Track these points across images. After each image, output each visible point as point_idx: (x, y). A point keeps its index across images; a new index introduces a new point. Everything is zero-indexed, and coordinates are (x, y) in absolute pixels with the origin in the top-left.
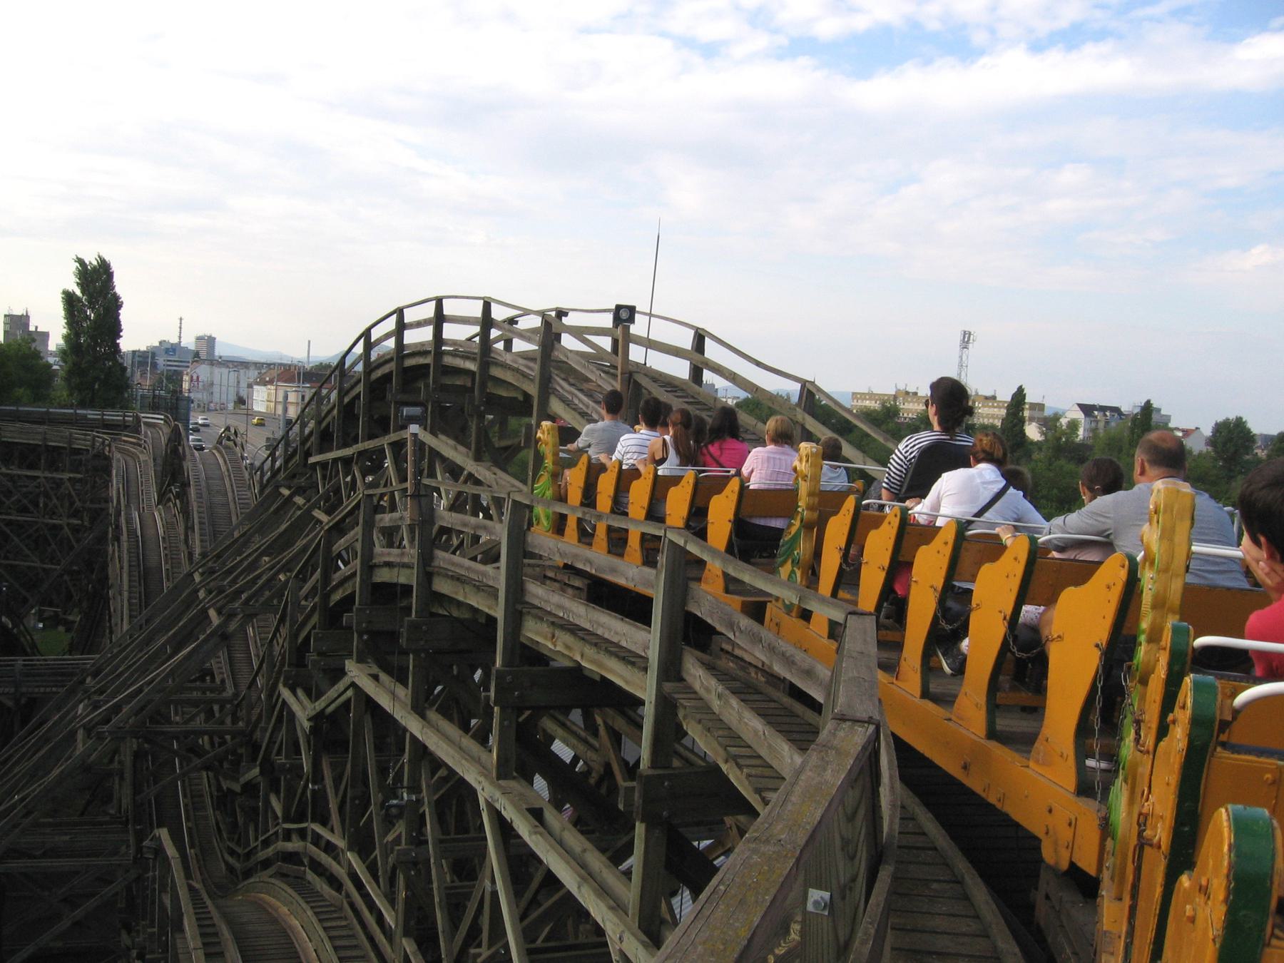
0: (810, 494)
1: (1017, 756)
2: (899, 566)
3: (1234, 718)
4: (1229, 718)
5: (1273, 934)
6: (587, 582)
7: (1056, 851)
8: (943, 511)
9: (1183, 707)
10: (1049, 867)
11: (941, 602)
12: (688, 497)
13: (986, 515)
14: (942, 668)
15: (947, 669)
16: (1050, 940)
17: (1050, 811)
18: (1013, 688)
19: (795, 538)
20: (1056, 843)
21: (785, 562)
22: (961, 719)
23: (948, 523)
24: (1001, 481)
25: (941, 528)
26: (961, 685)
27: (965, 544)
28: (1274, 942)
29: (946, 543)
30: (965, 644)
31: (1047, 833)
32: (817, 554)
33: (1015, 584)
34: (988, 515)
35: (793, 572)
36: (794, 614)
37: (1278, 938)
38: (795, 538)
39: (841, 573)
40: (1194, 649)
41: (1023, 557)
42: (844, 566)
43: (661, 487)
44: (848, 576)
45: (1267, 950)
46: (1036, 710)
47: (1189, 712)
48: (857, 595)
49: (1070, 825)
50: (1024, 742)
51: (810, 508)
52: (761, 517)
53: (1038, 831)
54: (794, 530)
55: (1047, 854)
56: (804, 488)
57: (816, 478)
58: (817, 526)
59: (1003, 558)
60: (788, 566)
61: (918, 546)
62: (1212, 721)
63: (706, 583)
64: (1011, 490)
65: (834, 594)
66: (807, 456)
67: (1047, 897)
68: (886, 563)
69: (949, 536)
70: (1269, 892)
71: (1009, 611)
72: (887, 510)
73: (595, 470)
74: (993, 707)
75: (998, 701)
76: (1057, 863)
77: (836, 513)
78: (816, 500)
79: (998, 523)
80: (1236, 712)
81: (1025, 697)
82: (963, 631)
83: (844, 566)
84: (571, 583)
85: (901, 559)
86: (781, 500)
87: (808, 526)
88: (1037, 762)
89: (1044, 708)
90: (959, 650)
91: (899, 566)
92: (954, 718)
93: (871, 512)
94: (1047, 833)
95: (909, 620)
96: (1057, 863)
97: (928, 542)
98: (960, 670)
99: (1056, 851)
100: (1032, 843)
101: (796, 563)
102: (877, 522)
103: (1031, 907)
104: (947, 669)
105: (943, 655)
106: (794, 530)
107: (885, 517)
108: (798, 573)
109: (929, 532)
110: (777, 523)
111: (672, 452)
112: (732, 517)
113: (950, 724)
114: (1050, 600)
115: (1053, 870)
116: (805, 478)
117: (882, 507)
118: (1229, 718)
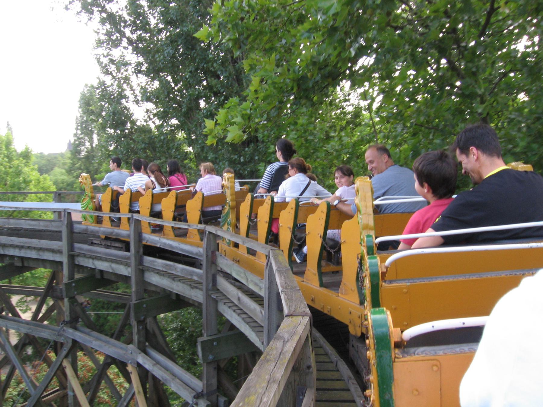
0: (231, 195)
1: (333, 292)
2: (273, 220)
3: (387, 270)
4: (385, 270)
5: (395, 357)
6: (124, 244)
7: (355, 329)
8: (287, 195)
9: (367, 270)
10: (352, 335)
11: (293, 232)
12: (174, 202)
13: (304, 194)
14: (296, 261)
15: (298, 261)
16: (355, 363)
17: (350, 313)
18: (327, 265)
19: (228, 213)
20: (354, 326)
21: (224, 224)
22: (308, 280)
23: (292, 200)
24: (305, 180)
25: (288, 202)
26: (306, 266)
27: (300, 208)
28: (396, 360)
29: (292, 209)
30: (305, 249)
31: (350, 322)
32: (238, 219)
33: (323, 222)
34: (305, 195)
35: (228, 228)
36: (231, 246)
37: (398, 358)
38: (228, 213)
39: (249, 226)
40: (376, 244)
41: (325, 210)
42: (250, 223)
43: (156, 199)
44: (252, 226)
45: (395, 364)
46: (338, 273)
47: (369, 271)
48: (257, 234)
49: (359, 317)
50: (335, 286)
51: (232, 200)
52: (210, 207)
53: (346, 322)
54: (226, 210)
55: (351, 330)
56: (228, 193)
57: (233, 187)
58: (236, 209)
59: (317, 212)
60: (226, 226)
61: (280, 211)
62: (378, 273)
63: (189, 238)
64: (312, 182)
65: (247, 236)
66: (228, 179)
67: (353, 346)
68: (268, 220)
69: (293, 205)
70: (389, 341)
71: (322, 233)
72: (265, 197)
73: (116, 196)
74: (321, 274)
75: (323, 271)
76: (356, 334)
77: (244, 201)
78: (234, 197)
79: (309, 197)
80: (387, 268)
81: (333, 267)
82: (304, 243)
83: (250, 223)
84: (113, 245)
85: (273, 217)
86: (220, 198)
87: (232, 208)
88: (342, 294)
89: (342, 271)
90: (302, 252)
91: (273, 220)
92: (305, 280)
93: (258, 199)
94: (350, 322)
95: (280, 243)
96: (356, 334)
97: (284, 209)
98: (304, 259)
99: (355, 329)
100: (345, 327)
101: (229, 224)
102: (261, 203)
103: (348, 351)
104: (298, 261)
105: (296, 255)
106: (226, 210)
107: (265, 200)
108: (231, 228)
109: (284, 204)
110: (218, 208)
111: (156, 184)
112: (200, 209)
113: (304, 283)
114: (339, 227)
115: (355, 337)
116: (228, 188)
117: (262, 196)
118: (385, 270)
